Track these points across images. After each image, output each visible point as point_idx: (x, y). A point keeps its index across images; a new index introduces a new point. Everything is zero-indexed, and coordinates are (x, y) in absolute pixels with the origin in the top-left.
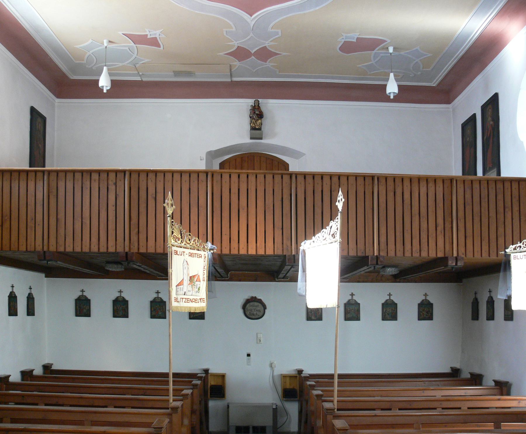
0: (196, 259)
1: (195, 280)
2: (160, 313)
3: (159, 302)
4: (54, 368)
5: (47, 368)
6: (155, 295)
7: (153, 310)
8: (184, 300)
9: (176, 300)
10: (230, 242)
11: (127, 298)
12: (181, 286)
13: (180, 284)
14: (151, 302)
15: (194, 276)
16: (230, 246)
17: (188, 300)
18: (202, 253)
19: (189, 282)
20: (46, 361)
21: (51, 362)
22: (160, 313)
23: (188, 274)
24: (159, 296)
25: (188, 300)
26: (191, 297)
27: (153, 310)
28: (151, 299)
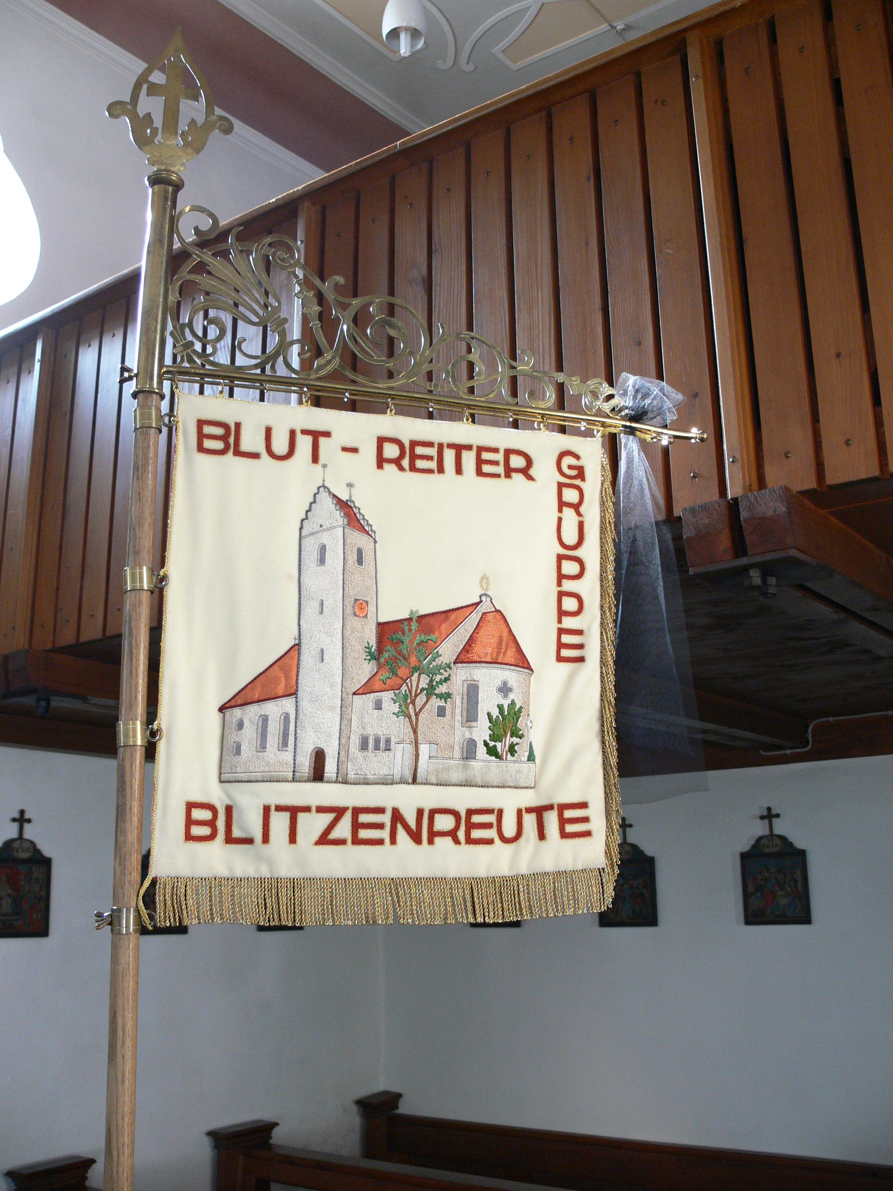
0: (461, 489)
1: (448, 649)
2: (784, 901)
3: (25, 861)
4: (405, 1108)
5: (379, 1113)
6: (760, 829)
7: (751, 888)
8: (312, 826)
9: (209, 822)
10: (877, 400)
11: (47, 850)
12: (274, 709)
13: (277, 681)
14: (744, 856)
15: (432, 624)
16: (879, 423)
17: (360, 825)
18: (542, 444)
19: (365, 670)
20: (382, 1084)
21: (395, 1089)
22: (784, 901)
23: (360, 607)
24: (778, 831)
25: (360, 825)
26: (409, 800)
27: (751, 888)
28: (745, 845)
